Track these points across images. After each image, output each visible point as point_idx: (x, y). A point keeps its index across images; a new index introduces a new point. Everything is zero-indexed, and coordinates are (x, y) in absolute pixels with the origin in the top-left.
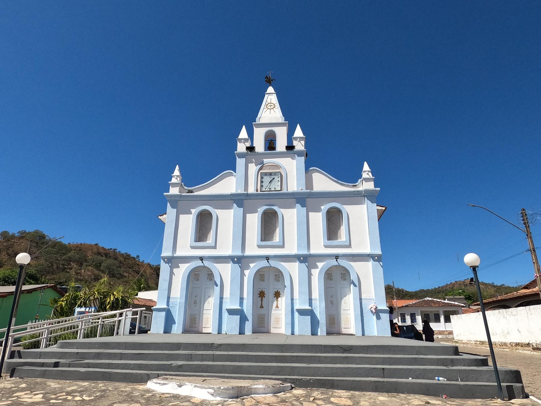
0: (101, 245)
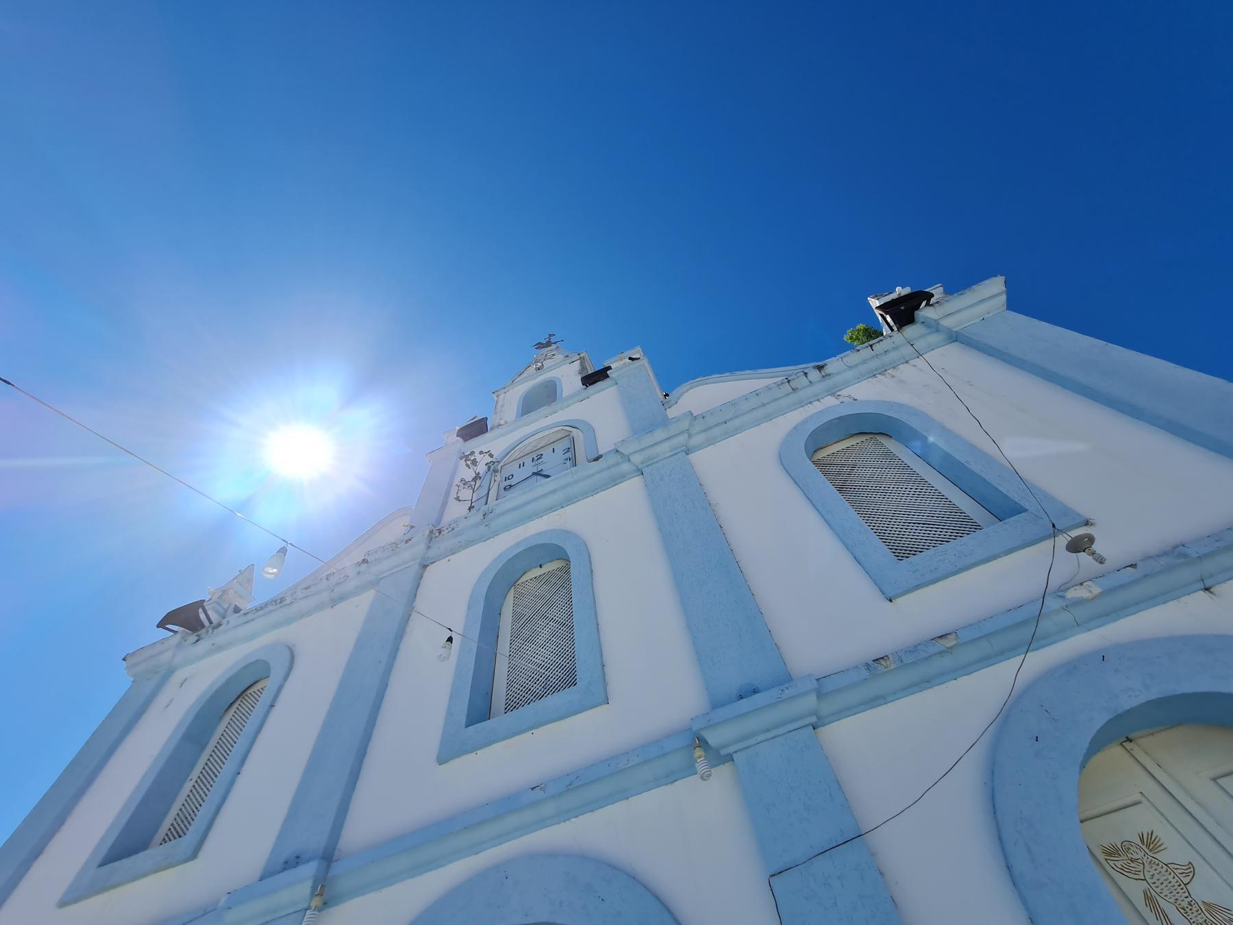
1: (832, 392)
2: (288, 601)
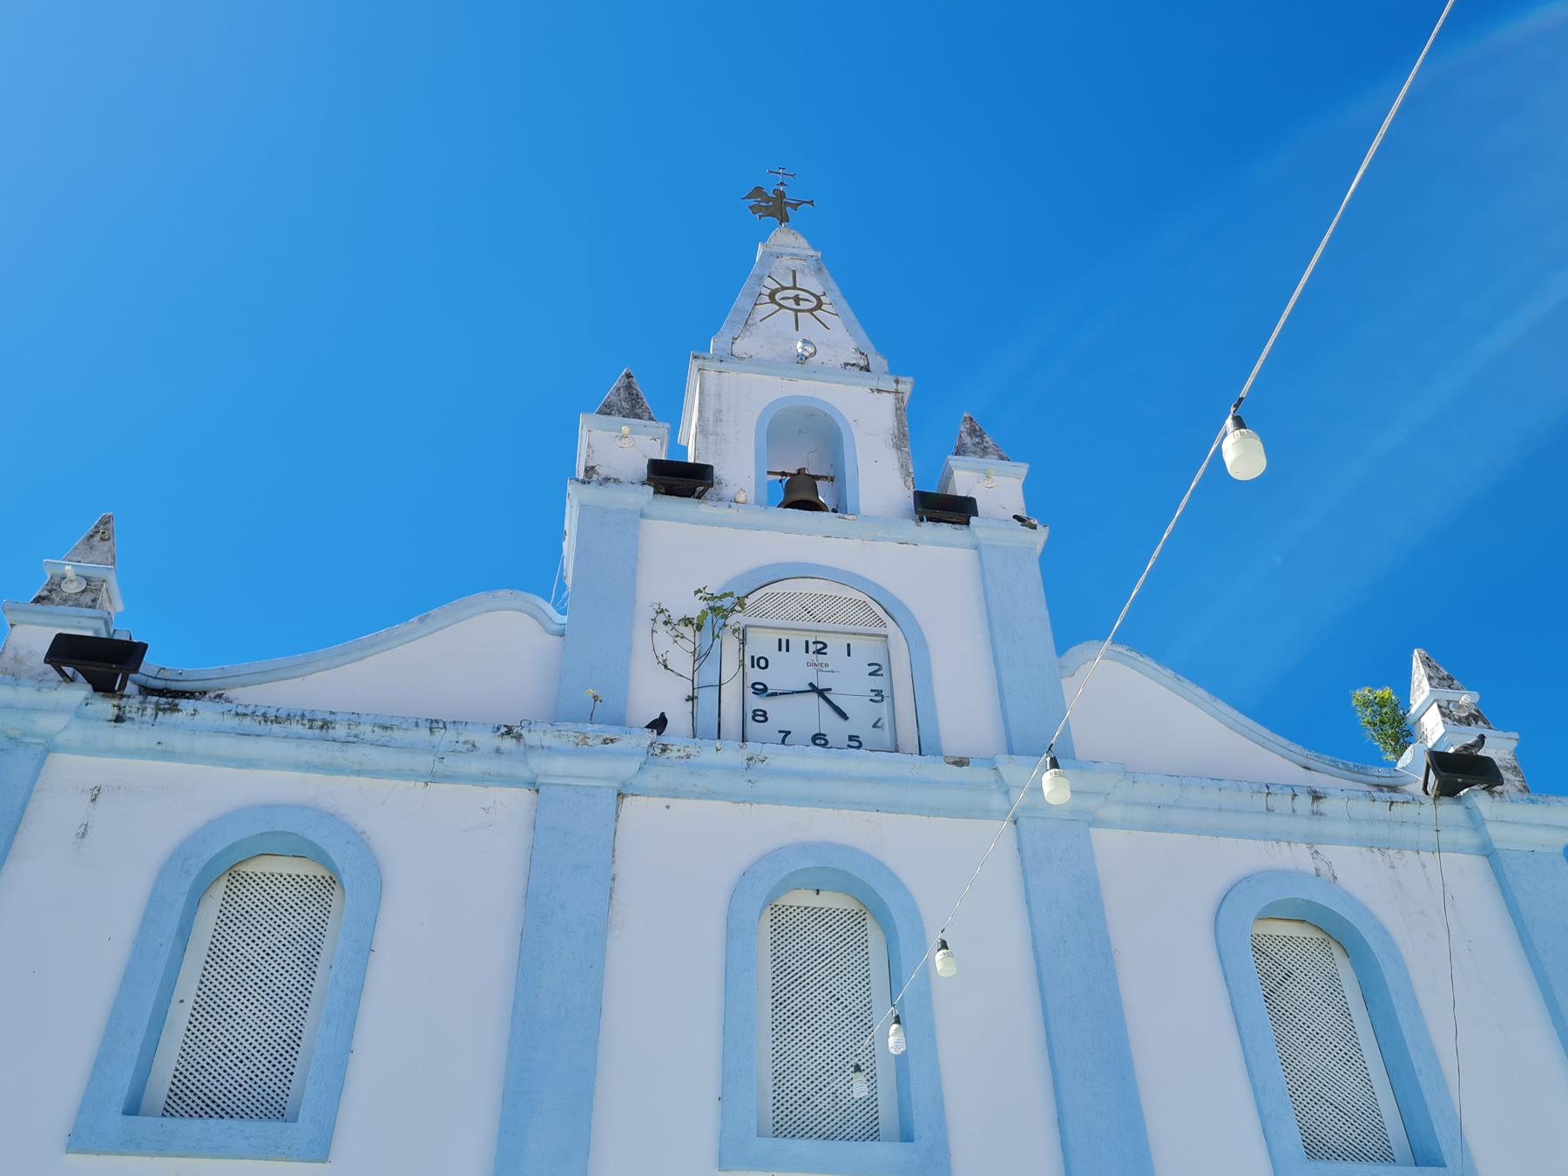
1: (1312, 841)
2: (340, 731)
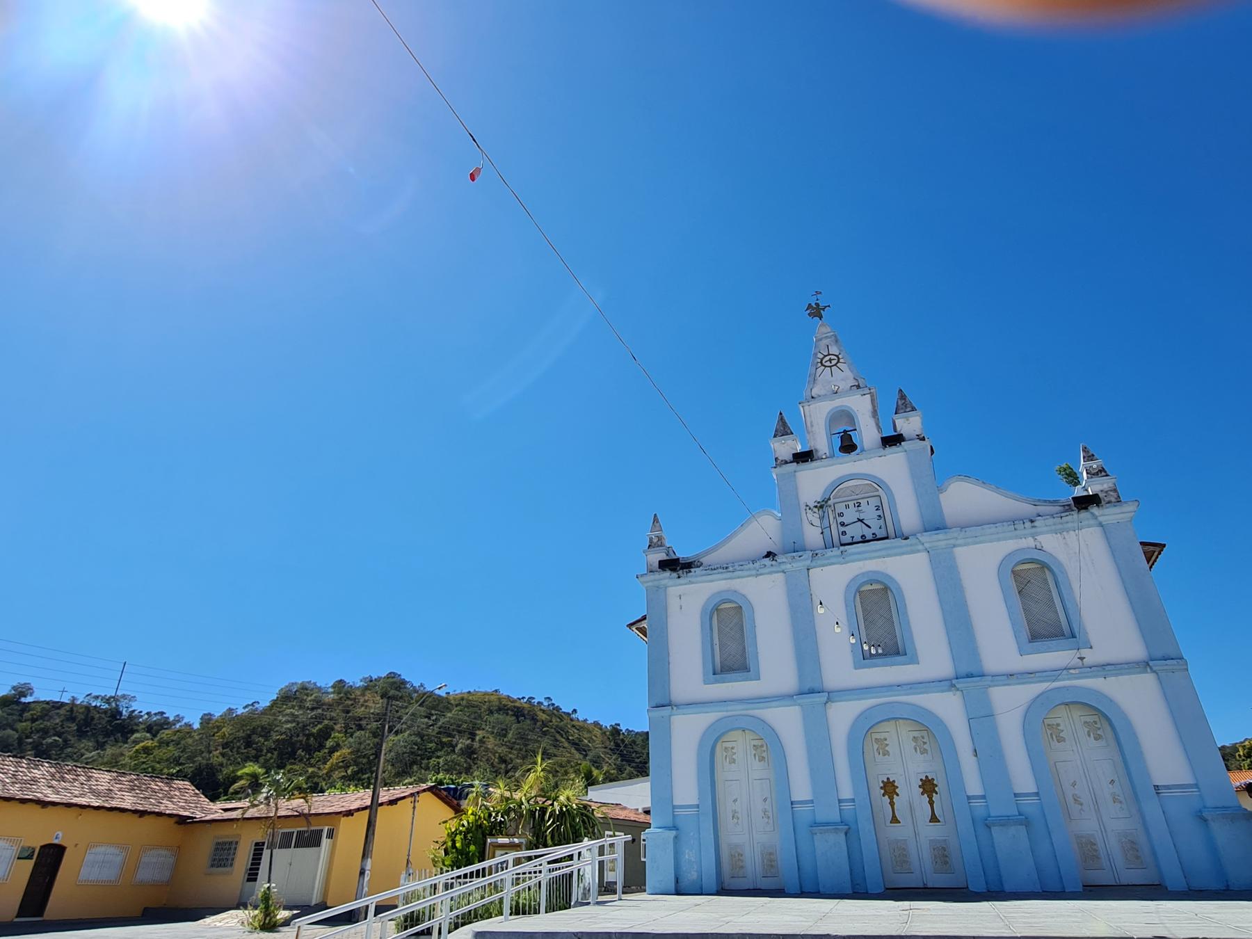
0: (504, 692)
1: (1033, 536)
